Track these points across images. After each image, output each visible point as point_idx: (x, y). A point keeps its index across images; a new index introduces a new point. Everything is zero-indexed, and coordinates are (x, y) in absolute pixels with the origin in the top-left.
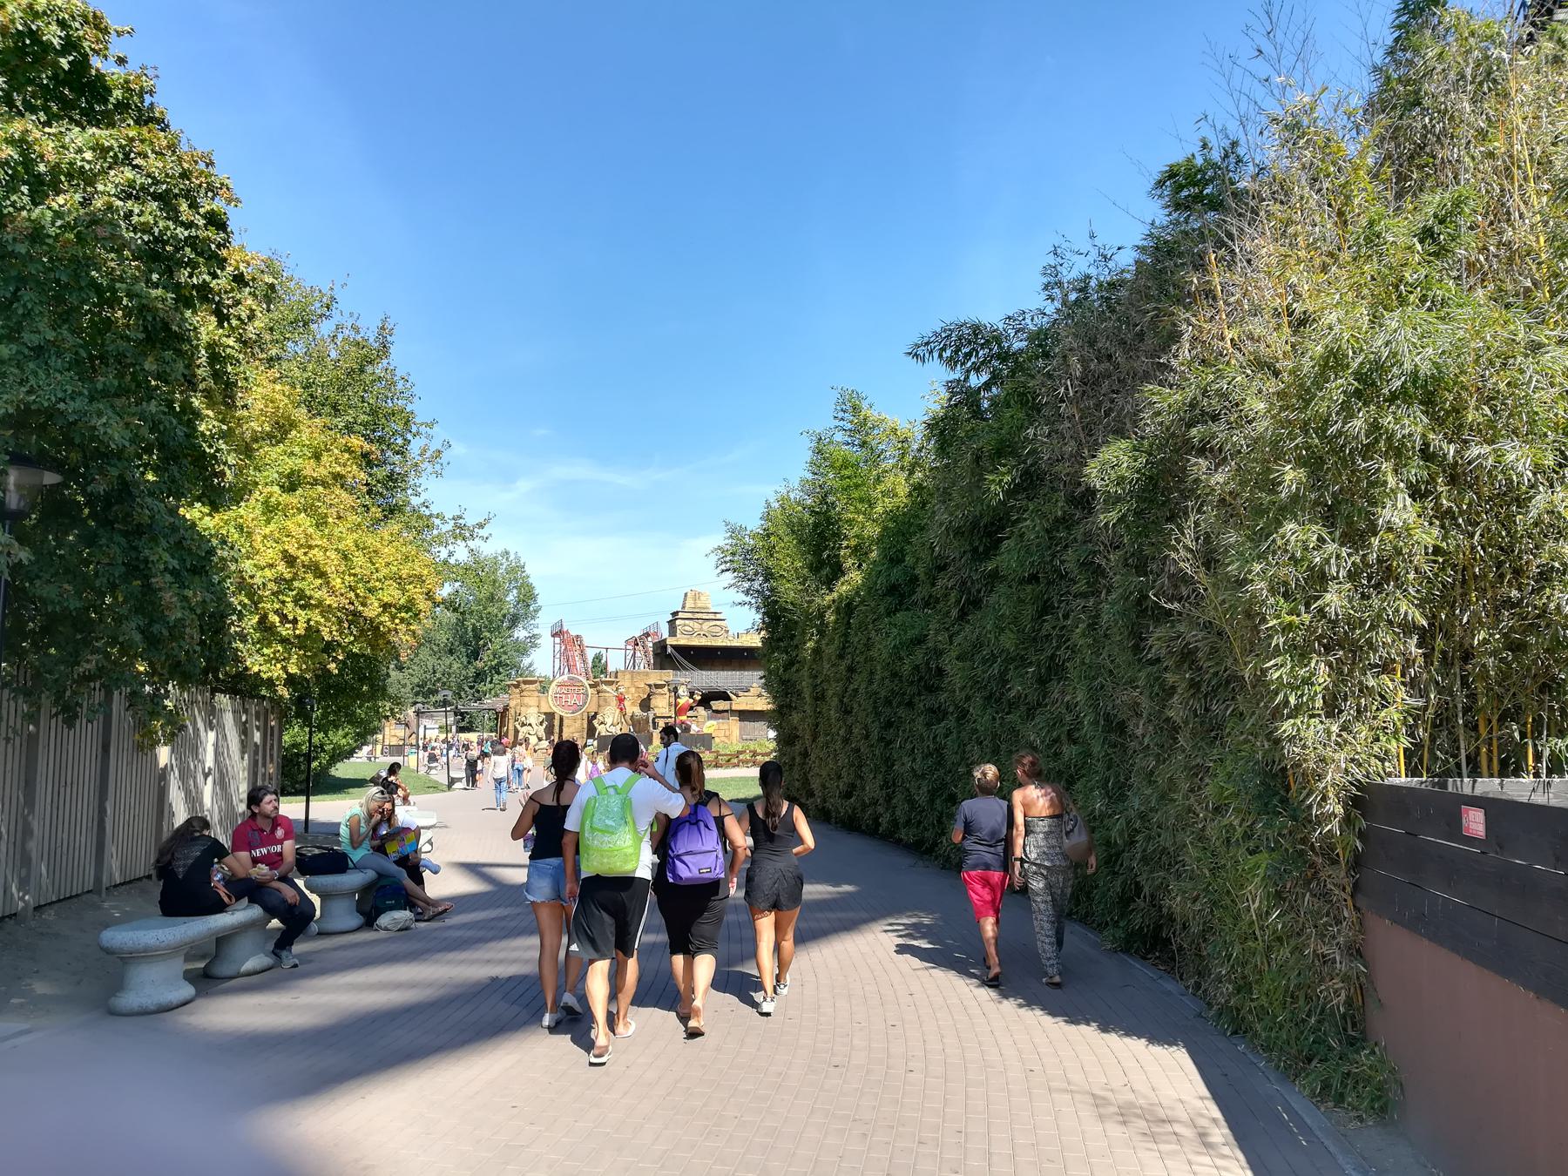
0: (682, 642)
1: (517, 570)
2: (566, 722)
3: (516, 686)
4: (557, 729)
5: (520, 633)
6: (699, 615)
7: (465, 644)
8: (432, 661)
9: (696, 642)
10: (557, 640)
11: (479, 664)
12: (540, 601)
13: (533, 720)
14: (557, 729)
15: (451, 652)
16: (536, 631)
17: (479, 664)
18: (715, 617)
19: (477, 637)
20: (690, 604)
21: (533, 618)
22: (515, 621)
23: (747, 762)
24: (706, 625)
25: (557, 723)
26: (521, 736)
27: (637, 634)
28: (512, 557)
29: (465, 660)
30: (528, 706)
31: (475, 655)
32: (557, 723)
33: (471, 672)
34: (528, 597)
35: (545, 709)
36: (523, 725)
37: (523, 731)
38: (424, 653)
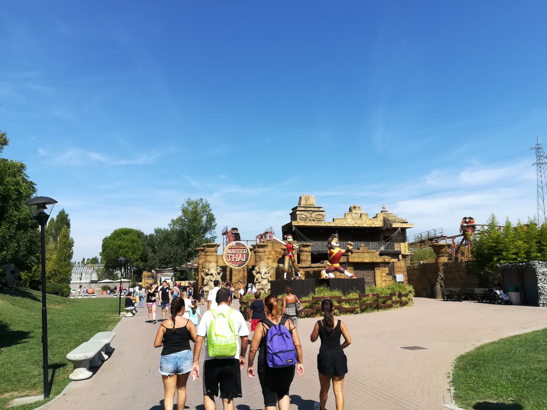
0: (302, 223)
1: (206, 207)
2: (234, 273)
3: (203, 251)
4: (228, 278)
5: (208, 236)
6: (309, 209)
7: (184, 241)
8: (169, 249)
9: (309, 224)
10: (225, 236)
11: (190, 249)
12: (217, 221)
13: (213, 271)
14: (228, 278)
15: (177, 244)
16: (215, 235)
17: (190, 249)
18: (319, 210)
19: (189, 237)
20: (303, 203)
21: (214, 229)
22: (206, 230)
23: (396, 302)
24: (314, 215)
25: (228, 273)
26: (205, 283)
27: (262, 233)
28: (204, 201)
29: (183, 248)
30: (210, 262)
31: (188, 245)
32: (228, 273)
33: (186, 253)
34: (211, 219)
35: (221, 264)
36: (207, 274)
37: (207, 278)
38: (165, 245)
